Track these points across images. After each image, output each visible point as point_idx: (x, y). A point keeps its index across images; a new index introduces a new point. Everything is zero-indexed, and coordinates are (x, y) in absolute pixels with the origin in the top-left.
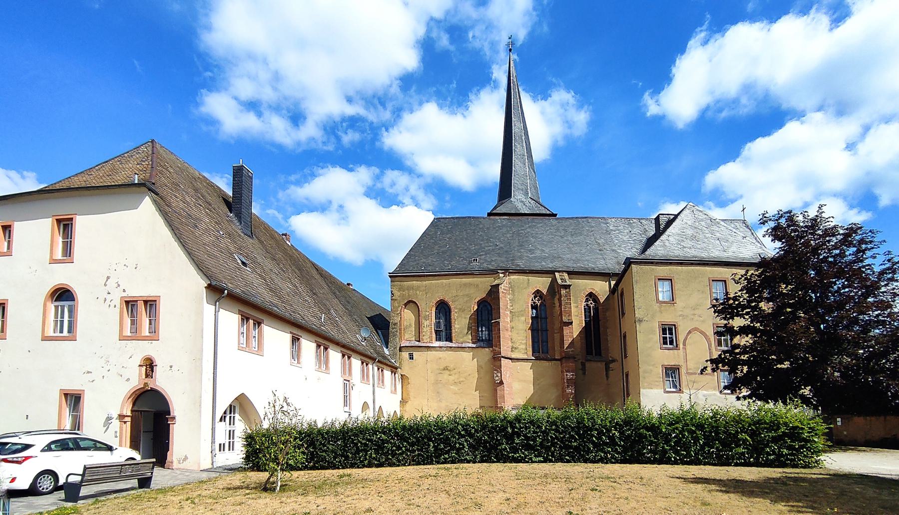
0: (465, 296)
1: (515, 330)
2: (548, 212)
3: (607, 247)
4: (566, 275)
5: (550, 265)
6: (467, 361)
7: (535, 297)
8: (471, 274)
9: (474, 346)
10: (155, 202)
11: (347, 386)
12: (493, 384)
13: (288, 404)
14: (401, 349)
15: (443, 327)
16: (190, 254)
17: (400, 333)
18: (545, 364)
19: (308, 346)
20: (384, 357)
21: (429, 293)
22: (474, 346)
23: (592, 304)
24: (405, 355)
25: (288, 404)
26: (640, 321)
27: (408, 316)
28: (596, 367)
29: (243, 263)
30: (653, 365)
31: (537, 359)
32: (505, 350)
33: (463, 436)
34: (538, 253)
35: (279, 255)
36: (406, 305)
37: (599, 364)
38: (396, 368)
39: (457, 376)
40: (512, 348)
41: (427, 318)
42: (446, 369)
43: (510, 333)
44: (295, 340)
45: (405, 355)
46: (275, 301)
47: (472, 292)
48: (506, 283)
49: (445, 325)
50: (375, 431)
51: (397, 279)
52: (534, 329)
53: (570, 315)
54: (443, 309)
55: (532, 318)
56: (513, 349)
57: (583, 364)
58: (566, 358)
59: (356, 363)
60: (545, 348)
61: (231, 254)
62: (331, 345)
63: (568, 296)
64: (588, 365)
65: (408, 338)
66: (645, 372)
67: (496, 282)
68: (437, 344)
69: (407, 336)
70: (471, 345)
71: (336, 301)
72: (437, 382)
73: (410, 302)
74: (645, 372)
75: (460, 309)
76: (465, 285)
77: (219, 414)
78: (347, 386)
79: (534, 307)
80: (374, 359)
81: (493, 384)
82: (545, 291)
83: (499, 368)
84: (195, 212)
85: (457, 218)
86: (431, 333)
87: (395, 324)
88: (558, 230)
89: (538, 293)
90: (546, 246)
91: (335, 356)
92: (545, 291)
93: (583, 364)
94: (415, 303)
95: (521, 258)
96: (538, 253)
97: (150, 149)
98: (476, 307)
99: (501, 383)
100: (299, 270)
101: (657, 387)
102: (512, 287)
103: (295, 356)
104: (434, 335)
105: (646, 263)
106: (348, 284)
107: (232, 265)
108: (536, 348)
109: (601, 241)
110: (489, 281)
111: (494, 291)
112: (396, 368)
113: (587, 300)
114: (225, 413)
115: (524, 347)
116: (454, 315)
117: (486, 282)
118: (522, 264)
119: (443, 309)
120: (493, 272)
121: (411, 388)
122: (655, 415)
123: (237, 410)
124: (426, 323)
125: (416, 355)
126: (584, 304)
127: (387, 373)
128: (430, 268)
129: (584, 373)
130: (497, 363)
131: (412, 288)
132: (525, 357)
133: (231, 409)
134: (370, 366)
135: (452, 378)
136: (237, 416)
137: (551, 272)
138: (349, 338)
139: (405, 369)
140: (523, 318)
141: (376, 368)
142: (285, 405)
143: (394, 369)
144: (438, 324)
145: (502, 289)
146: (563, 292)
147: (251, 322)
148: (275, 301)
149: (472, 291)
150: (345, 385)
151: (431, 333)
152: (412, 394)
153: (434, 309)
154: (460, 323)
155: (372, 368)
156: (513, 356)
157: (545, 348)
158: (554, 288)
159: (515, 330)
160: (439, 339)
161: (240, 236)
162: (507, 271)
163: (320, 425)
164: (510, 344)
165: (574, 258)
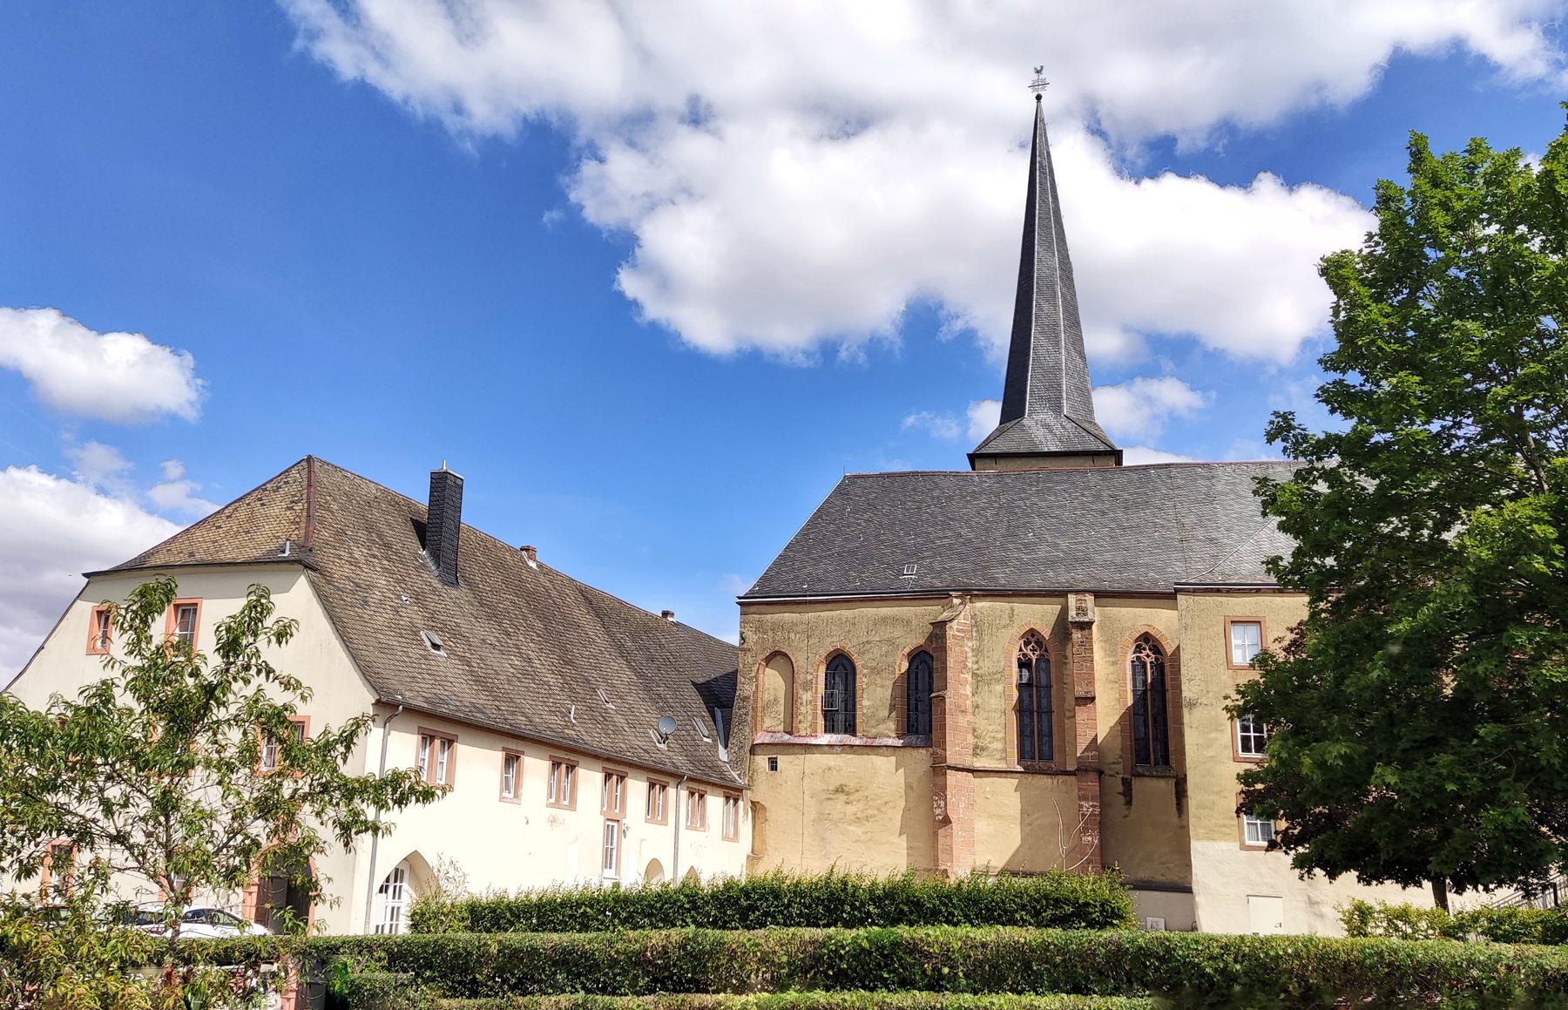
0: (882, 638)
1: (981, 710)
2: (1102, 448)
3: (1200, 533)
4: (1090, 599)
5: (1061, 578)
6: (886, 775)
7: (1027, 644)
8: (898, 597)
9: (899, 743)
10: (313, 584)
11: (613, 827)
12: (932, 821)
13: (456, 869)
14: (753, 750)
15: (839, 705)
16: (355, 657)
17: (754, 718)
18: (1045, 781)
19: (535, 767)
20: (715, 767)
21: (816, 632)
22: (899, 743)
23: (1148, 657)
24: (762, 761)
25: (456, 869)
26: (1192, 705)
27: (772, 681)
28: (1153, 789)
29: (436, 647)
30: (1217, 793)
31: (1028, 771)
32: (956, 752)
33: (689, 910)
34: (1043, 552)
35: (507, 600)
36: (768, 660)
37: (1162, 783)
38: (740, 790)
39: (861, 805)
40: (976, 747)
41: (808, 686)
42: (840, 790)
43: (970, 717)
44: (511, 760)
45: (762, 761)
46: (482, 699)
47: (897, 634)
48: (963, 617)
49: (846, 701)
50: (578, 905)
51: (753, 609)
52: (1022, 710)
53: (1091, 682)
54: (841, 667)
55: (1020, 686)
56: (977, 750)
57: (1127, 784)
58: (1092, 768)
59: (636, 788)
60: (1045, 748)
61: (416, 634)
62: (582, 760)
63: (1087, 645)
64: (1137, 784)
65: (769, 727)
66: (1201, 806)
67: (945, 615)
68: (825, 739)
69: (768, 723)
70: (890, 742)
71: (617, 665)
72: (822, 817)
73: (776, 654)
74: (1201, 806)
75: (873, 669)
76: (884, 620)
77: (379, 881)
78: (613, 827)
79: (1024, 664)
80: (678, 777)
81: (932, 821)
82: (1046, 633)
83: (940, 791)
84: (366, 574)
85: (889, 475)
86: (815, 715)
87: (745, 699)
88: (1098, 497)
89: (1031, 637)
90: (1063, 534)
91: (590, 779)
92: (1046, 633)
93: (1127, 784)
94: (785, 655)
95: (1003, 563)
96: (1043, 552)
97: (304, 474)
98: (905, 666)
99: (946, 821)
100: (543, 618)
101: (1226, 837)
102: (977, 624)
103: (512, 784)
104: (821, 722)
105: (1206, 591)
106: (665, 614)
107: (415, 652)
108: (1027, 748)
109: (1190, 520)
110: (930, 611)
111: (939, 629)
112: (740, 790)
113: (1139, 649)
114: (388, 880)
115: (999, 745)
116: (862, 681)
117: (922, 614)
118: (1002, 578)
119: (841, 667)
120: (941, 595)
121: (771, 832)
122: (704, 883)
123: (406, 875)
124: (806, 696)
125: (783, 761)
126: (1131, 656)
127: (715, 802)
128: (818, 587)
129: (1129, 803)
130: (939, 780)
131: (782, 626)
132: (1002, 766)
133: (398, 874)
134: (671, 791)
135: (851, 809)
136: (405, 886)
137: (1063, 594)
138: (630, 742)
139: (761, 792)
140: (999, 688)
141: (684, 794)
142: (451, 870)
143: (732, 793)
144: (829, 699)
145: (952, 630)
146: (1077, 635)
147: (437, 742)
148: (482, 699)
149: (898, 632)
150: (609, 831)
151: (815, 715)
152: (770, 842)
153: (823, 669)
154: (876, 697)
155: (677, 796)
156: (979, 763)
157: (1045, 748)
158: (1063, 627)
159: (981, 710)
160: (830, 728)
161: (434, 590)
162: (969, 593)
163: (512, 897)
164: (971, 740)
165: (1119, 560)
